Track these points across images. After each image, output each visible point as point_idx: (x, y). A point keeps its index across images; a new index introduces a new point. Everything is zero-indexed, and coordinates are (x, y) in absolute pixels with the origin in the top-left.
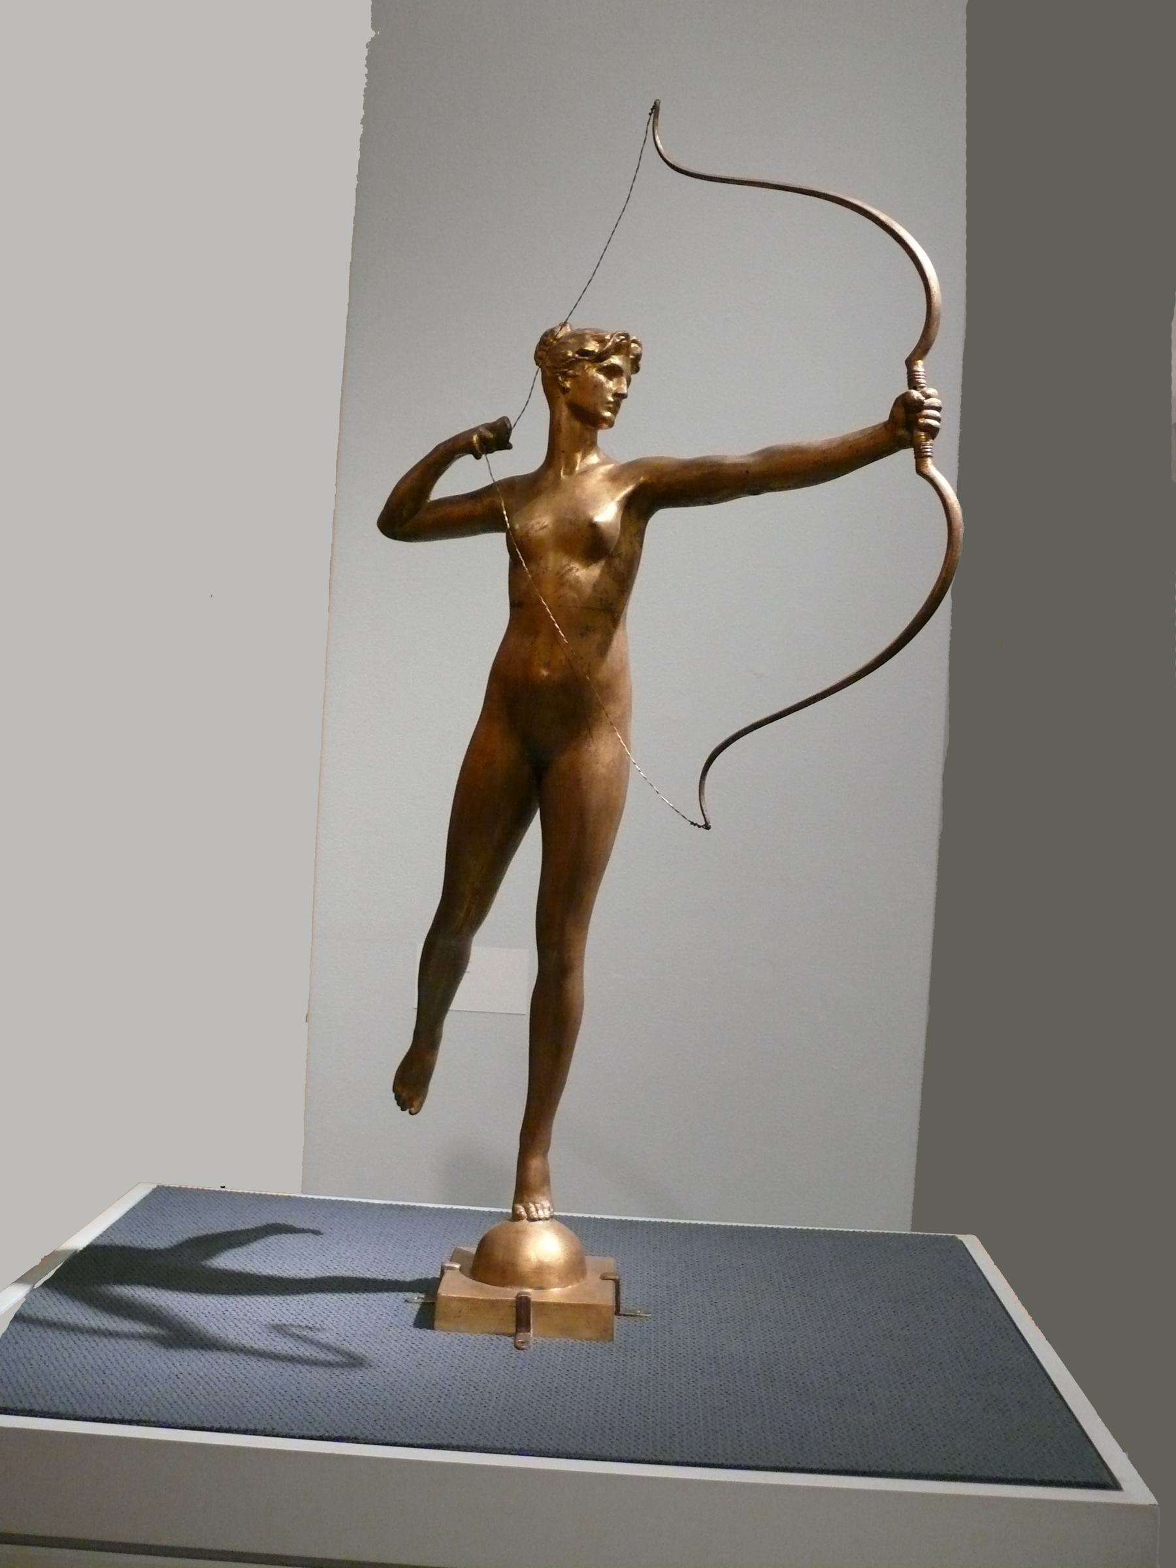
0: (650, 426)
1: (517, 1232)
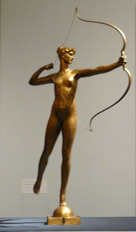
0: (79, 63)
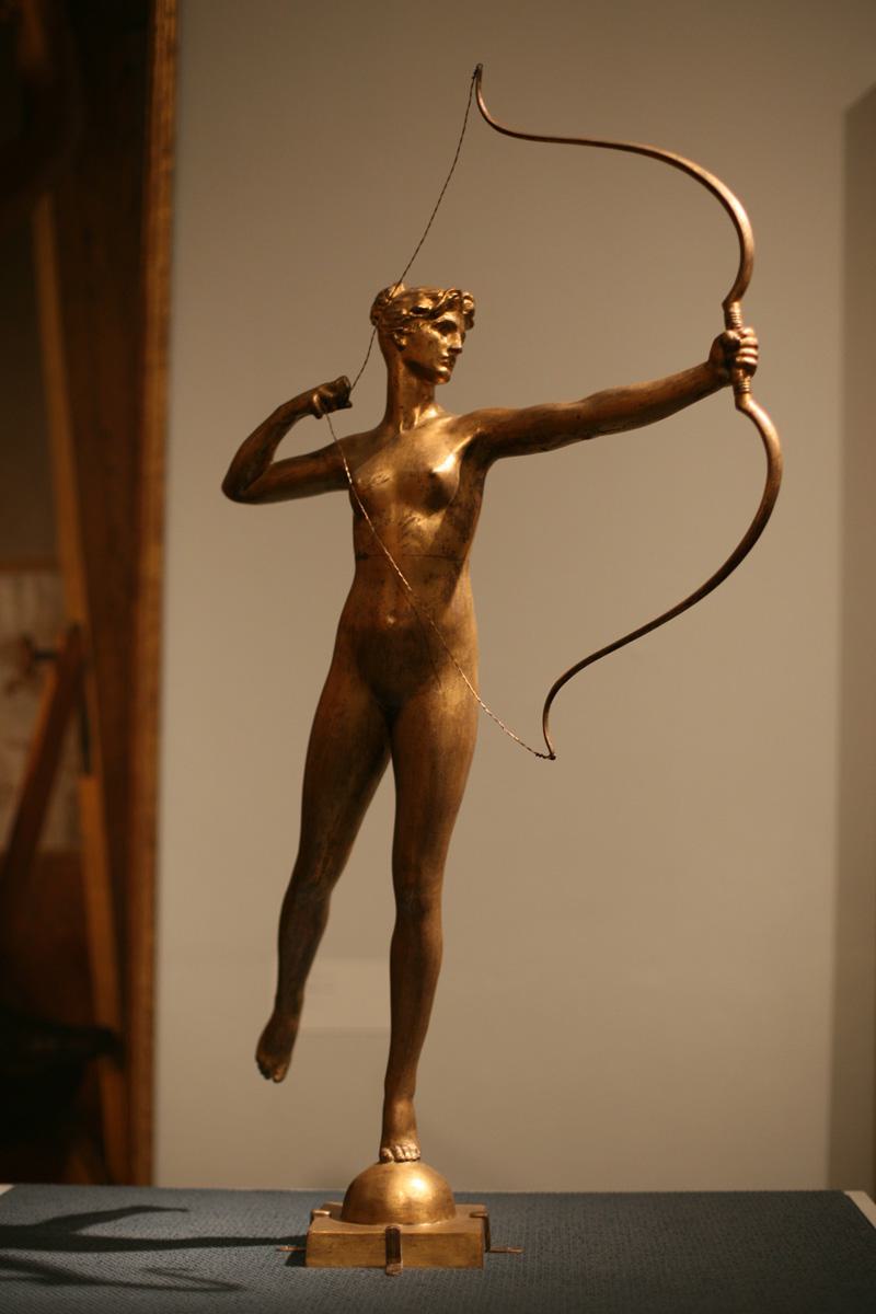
0: (495, 374)
1: (385, 1172)
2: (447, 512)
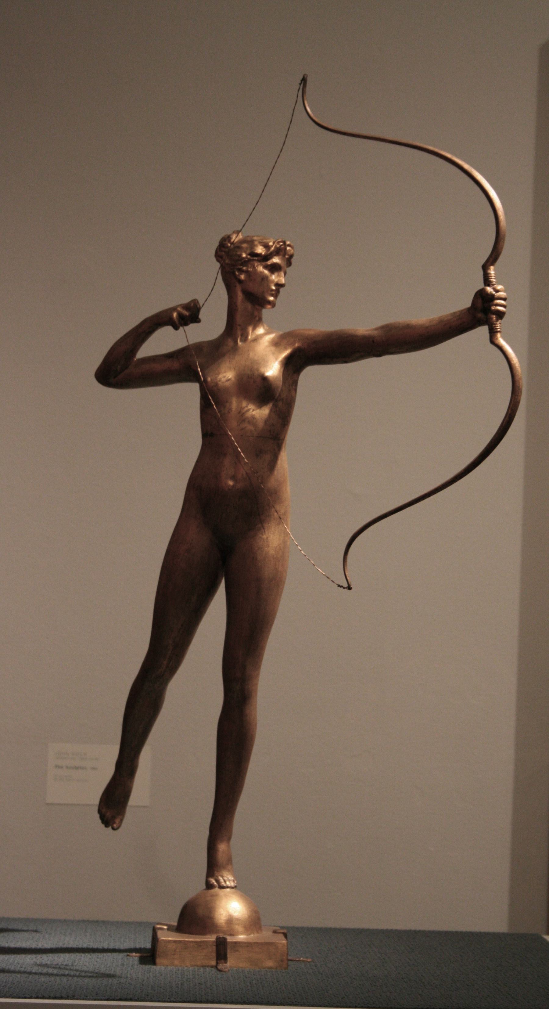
0: (308, 301)
1: (212, 896)
2: (273, 405)
